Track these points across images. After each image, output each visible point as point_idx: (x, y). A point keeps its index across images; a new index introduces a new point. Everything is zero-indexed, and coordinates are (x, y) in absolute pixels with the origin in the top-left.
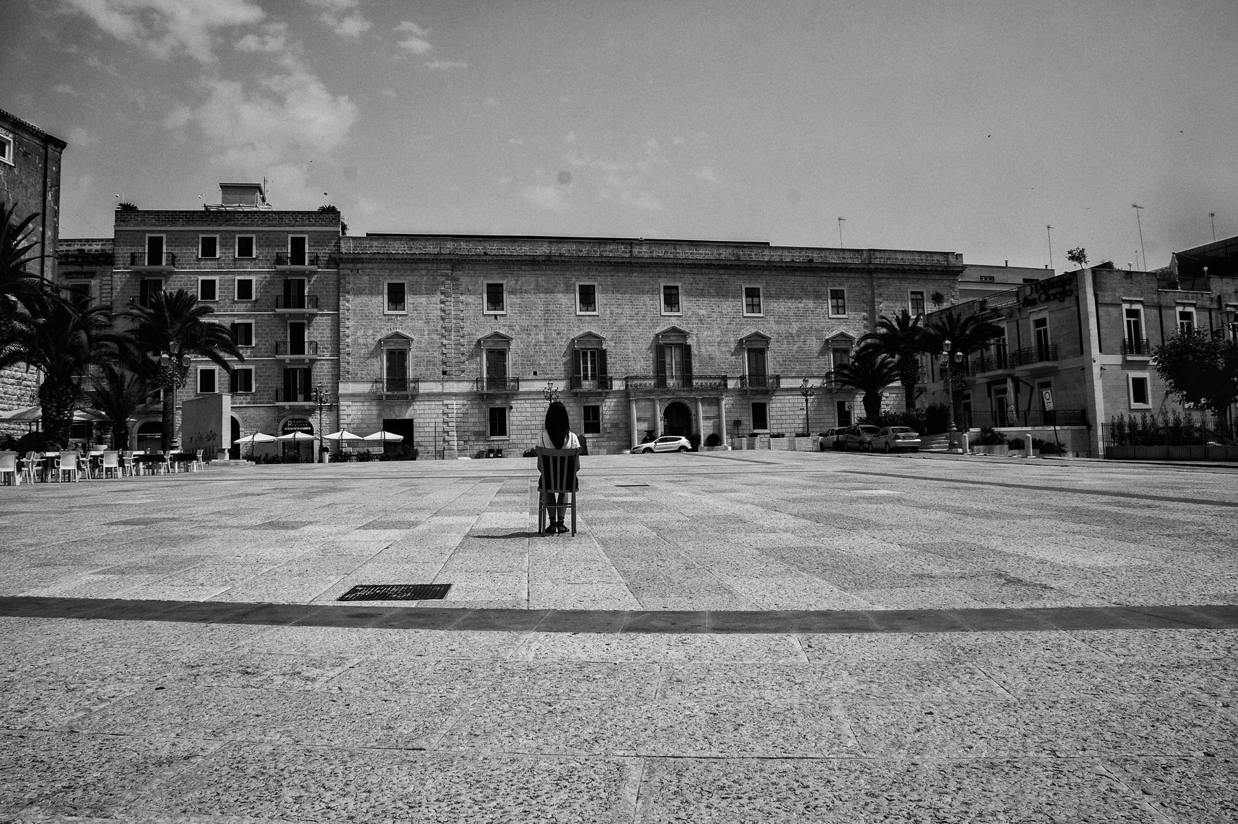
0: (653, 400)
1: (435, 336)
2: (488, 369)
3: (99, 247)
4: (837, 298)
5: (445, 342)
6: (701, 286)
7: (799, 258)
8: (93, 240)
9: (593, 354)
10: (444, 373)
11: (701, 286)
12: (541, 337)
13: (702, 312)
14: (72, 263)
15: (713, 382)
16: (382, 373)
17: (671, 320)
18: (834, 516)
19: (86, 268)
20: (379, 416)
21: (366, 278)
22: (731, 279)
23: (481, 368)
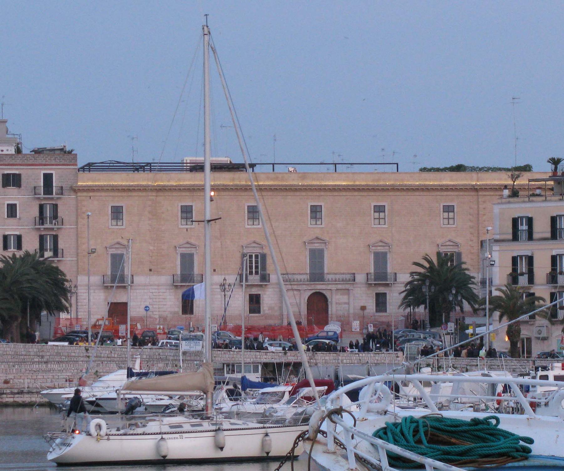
20: (106, 299)
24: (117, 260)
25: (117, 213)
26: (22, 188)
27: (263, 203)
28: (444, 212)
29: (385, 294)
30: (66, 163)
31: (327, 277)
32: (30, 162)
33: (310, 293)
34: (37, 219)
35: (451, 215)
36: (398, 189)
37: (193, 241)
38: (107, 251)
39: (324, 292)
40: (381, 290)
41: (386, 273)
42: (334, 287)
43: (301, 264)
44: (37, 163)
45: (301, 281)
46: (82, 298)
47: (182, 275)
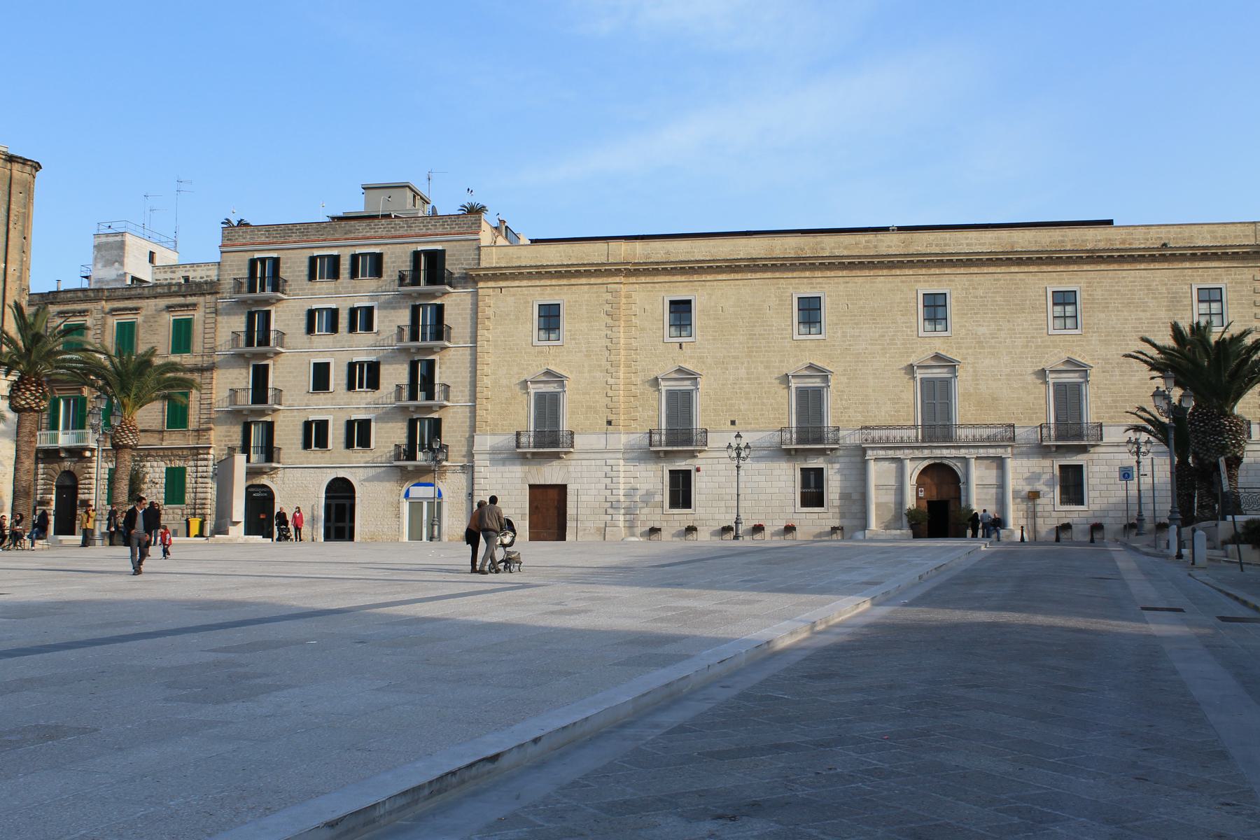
0: (899, 461)
1: (598, 374)
2: (668, 417)
3: (204, 274)
4: (1064, 304)
5: (611, 381)
6: (980, 292)
7: (1152, 240)
8: (198, 265)
9: (75, 401)
10: (609, 423)
11: (980, 292)
12: (742, 372)
13: (982, 330)
14: (176, 294)
15: (994, 431)
16: (1047, 416)
17: (938, 343)
18: (51, 738)
19: (190, 300)
20: (523, 479)
21: (510, 300)
22: (1030, 279)
23: (659, 416)
24: (548, 407)
25: (550, 318)
26: (385, 277)
27: (705, 296)
28: (1055, 304)
29: (1079, 468)
30: (461, 230)
31: (961, 433)
32: (401, 232)
33: (923, 465)
34: (243, 337)
35: (1069, 310)
36: (1216, 254)
37: (688, 366)
38: (527, 388)
39: (951, 463)
40: (681, 465)
41: (821, 428)
42: (970, 453)
43: (900, 407)
44: (412, 233)
45: (888, 440)
46: (482, 475)
47: (670, 432)
